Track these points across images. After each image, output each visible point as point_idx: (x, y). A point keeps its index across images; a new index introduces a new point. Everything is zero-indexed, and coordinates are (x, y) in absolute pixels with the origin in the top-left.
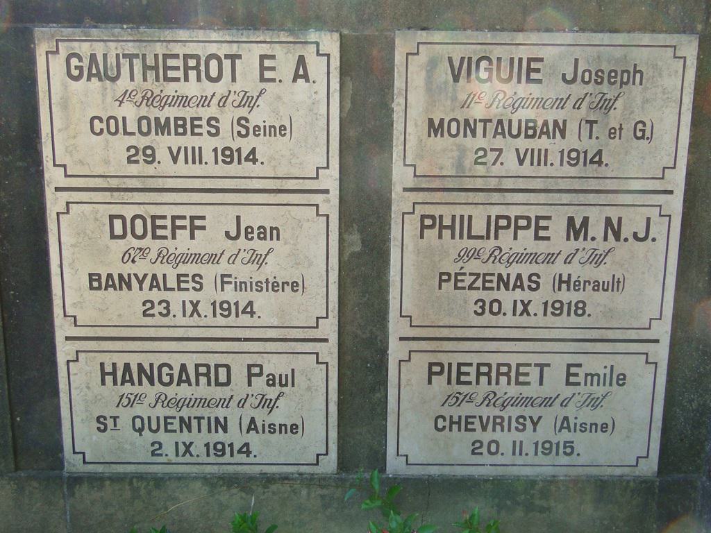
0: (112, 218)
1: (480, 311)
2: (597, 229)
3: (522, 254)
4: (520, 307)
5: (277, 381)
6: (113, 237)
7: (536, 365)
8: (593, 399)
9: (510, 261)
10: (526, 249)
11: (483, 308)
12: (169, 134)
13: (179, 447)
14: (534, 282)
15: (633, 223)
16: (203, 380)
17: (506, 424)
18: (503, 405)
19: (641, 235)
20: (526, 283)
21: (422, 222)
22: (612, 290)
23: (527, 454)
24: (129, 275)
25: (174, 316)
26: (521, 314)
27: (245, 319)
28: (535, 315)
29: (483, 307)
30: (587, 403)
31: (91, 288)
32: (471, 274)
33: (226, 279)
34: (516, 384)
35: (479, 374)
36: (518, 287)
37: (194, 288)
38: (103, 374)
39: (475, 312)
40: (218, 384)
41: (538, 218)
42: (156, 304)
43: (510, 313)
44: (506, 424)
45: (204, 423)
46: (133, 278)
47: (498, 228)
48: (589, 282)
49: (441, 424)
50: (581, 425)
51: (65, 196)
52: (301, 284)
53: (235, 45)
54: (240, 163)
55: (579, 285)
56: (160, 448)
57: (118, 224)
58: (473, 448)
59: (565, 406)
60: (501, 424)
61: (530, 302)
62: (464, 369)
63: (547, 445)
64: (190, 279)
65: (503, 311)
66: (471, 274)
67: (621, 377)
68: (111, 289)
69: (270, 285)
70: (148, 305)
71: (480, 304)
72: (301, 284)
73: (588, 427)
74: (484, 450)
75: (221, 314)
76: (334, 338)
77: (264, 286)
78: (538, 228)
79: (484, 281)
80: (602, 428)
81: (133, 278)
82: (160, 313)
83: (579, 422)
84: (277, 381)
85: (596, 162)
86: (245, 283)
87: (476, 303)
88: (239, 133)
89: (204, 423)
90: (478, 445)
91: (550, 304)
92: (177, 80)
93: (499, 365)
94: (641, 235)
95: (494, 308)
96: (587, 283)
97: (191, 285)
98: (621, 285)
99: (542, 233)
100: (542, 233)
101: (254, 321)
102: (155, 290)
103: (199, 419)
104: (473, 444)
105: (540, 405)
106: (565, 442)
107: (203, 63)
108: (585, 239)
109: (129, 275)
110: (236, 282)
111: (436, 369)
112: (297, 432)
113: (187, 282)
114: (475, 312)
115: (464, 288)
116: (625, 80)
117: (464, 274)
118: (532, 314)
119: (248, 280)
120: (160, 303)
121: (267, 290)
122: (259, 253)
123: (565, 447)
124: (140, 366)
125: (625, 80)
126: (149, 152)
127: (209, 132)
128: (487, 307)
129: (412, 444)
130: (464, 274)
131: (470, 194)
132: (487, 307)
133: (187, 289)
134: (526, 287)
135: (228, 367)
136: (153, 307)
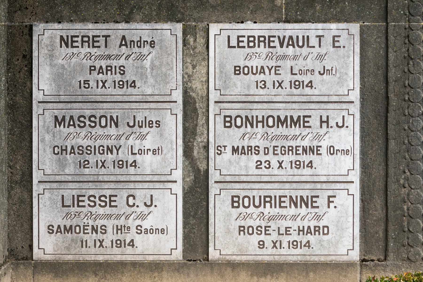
3: (279, 136)
9: (96, 139)
10: (281, 133)
13: (279, 246)
14: (80, 150)
15: (336, 118)
18: (268, 220)
19: (340, 124)
21: (225, 119)
22: (144, 154)
24: (112, 146)
25: (315, 168)
28: (286, 168)
30: (138, 218)
38: (322, 122)
42: (263, 163)
46: (114, 147)
48: (150, 150)
60: (111, 70)
61: (283, 161)
62: (283, 199)
68: (243, 155)
70: (259, 163)
80: (161, 231)
81: (114, 147)
82: (265, 167)
85: (309, 86)
91: (294, 162)
94: (340, 124)
96: (338, 151)
98: (160, 151)
105: (290, 220)
106: (85, 81)
109: (112, 146)
111: (93, 68)
112: (164, 233)
116: (139, 43)
120: (265, 162)
123: (84, 84)
125: (139, 43)
129: (226, 240)
134: (76, 153)
136: (261, 164)
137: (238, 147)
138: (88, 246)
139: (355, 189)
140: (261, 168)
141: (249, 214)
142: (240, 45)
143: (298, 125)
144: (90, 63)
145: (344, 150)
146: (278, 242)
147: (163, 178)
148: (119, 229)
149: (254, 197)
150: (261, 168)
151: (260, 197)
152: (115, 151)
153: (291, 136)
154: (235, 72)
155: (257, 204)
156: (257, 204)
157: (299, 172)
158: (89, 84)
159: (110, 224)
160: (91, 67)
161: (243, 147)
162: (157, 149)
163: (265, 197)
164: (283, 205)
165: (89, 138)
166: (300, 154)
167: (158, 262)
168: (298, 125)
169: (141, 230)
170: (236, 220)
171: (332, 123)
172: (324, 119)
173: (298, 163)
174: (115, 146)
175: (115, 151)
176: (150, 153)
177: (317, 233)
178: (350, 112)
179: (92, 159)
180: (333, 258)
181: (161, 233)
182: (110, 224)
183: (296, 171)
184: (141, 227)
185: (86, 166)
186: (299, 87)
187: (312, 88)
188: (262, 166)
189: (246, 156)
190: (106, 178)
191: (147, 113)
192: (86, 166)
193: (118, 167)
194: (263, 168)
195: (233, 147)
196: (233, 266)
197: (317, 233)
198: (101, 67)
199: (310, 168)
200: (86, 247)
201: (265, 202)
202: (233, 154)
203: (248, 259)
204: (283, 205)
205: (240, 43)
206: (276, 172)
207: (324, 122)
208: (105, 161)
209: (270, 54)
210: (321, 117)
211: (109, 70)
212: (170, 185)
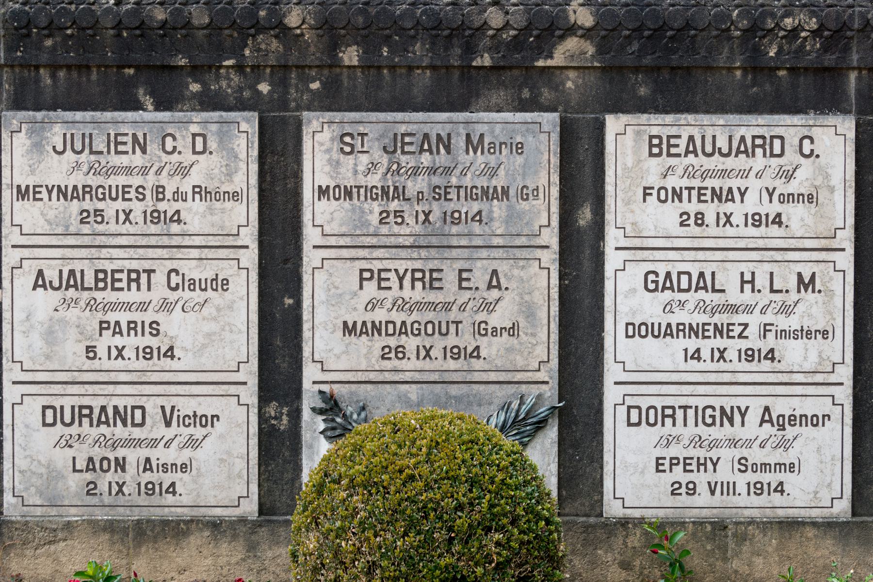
4: (717, 355)
5: (213, 195)
9: (106, 309)
12: (28, 200)
17: (139, 329)
23: (739, 494)
26: (116, 358)
28: (129, 359)
32: (739, 324)
33: (768, 328)
35: (130, 280)
36: (669, 335)
38: (743, 282)
40: (134, 425)
41: (380, 271)
42: (684, 486)
43: (413, 356)
44: (139, 329)
45: (691, 413)
48: (819, 331)
50: (163, 466)
53: (675, 128)
54: (767, 226)
56: (95, 488)
58: (86, 489)
60: (135, 329)
63: (150, 486)
66: (739, 324)
67: (792, 418)
68: (364, 336)
69: (804, 332)
73: (169, 467)
75: (746, 359)
76: (849, 383)
77: (799, 334)
78: (380, 279)
80: (182, 468)
83: (161, 462)
84: (213, 195)
86: (785, 331)
88: (434, 197)
89: (691, 413)
92: (126, 153)
93: (663, 408)
95: (400, 352)
99: (383, 284)
100: (383, 284)
103: (685, 408)
107: (768, 141)
108: (813, 291)
110: (777, 331)
115: (733, 337)
117: (734, 324)
118: (433, 358)
119: (787, 329)
121: (802, 338)
122: (169, 301)
124: (115, 408)
127: (137, 197)
130: (734, 324)
131: (707, 252)
133: (130, 200)
135: (143, 408)
137: (355, 323)
138: (737, 493)
139: (250, 257)
140: (680, 494)
142: (406, 150)
143: (810, 288)
144: (100, 316)
146: (716, 359)
148: (702, 464)
149: (62, 407)
151: (73, 407)
155: (68, 419)
156: (68, 419)
158: (102, 216)
159: (133, 456)
160: (101, 322)
161: (364, 323)
163: (81, 407)
166: (709, 337)
168: (810, 288)
169: (746, 466)
172: (748, 277)
176: (819, 336)
177: (681, 334)
181: (181, 471)
182: (133, 456)
183: (746, 366)
184: (747, 460)
185: (386, 356)
186: (459, 357)
187: (780, 226)
190: (484, 377)
192: (386, 356)
193: (144, 357)
194: (684, 494)
195: (345, 323)
197: (681, 334)
198: (117, 323)
200: (734, 494)
201: (81, 416)
202: (344, 335)
205: (672, 149)
206: (107, 364)
208: (431, 347)
210: (742, 274)
211: (197, 193)
212: (24, 241)
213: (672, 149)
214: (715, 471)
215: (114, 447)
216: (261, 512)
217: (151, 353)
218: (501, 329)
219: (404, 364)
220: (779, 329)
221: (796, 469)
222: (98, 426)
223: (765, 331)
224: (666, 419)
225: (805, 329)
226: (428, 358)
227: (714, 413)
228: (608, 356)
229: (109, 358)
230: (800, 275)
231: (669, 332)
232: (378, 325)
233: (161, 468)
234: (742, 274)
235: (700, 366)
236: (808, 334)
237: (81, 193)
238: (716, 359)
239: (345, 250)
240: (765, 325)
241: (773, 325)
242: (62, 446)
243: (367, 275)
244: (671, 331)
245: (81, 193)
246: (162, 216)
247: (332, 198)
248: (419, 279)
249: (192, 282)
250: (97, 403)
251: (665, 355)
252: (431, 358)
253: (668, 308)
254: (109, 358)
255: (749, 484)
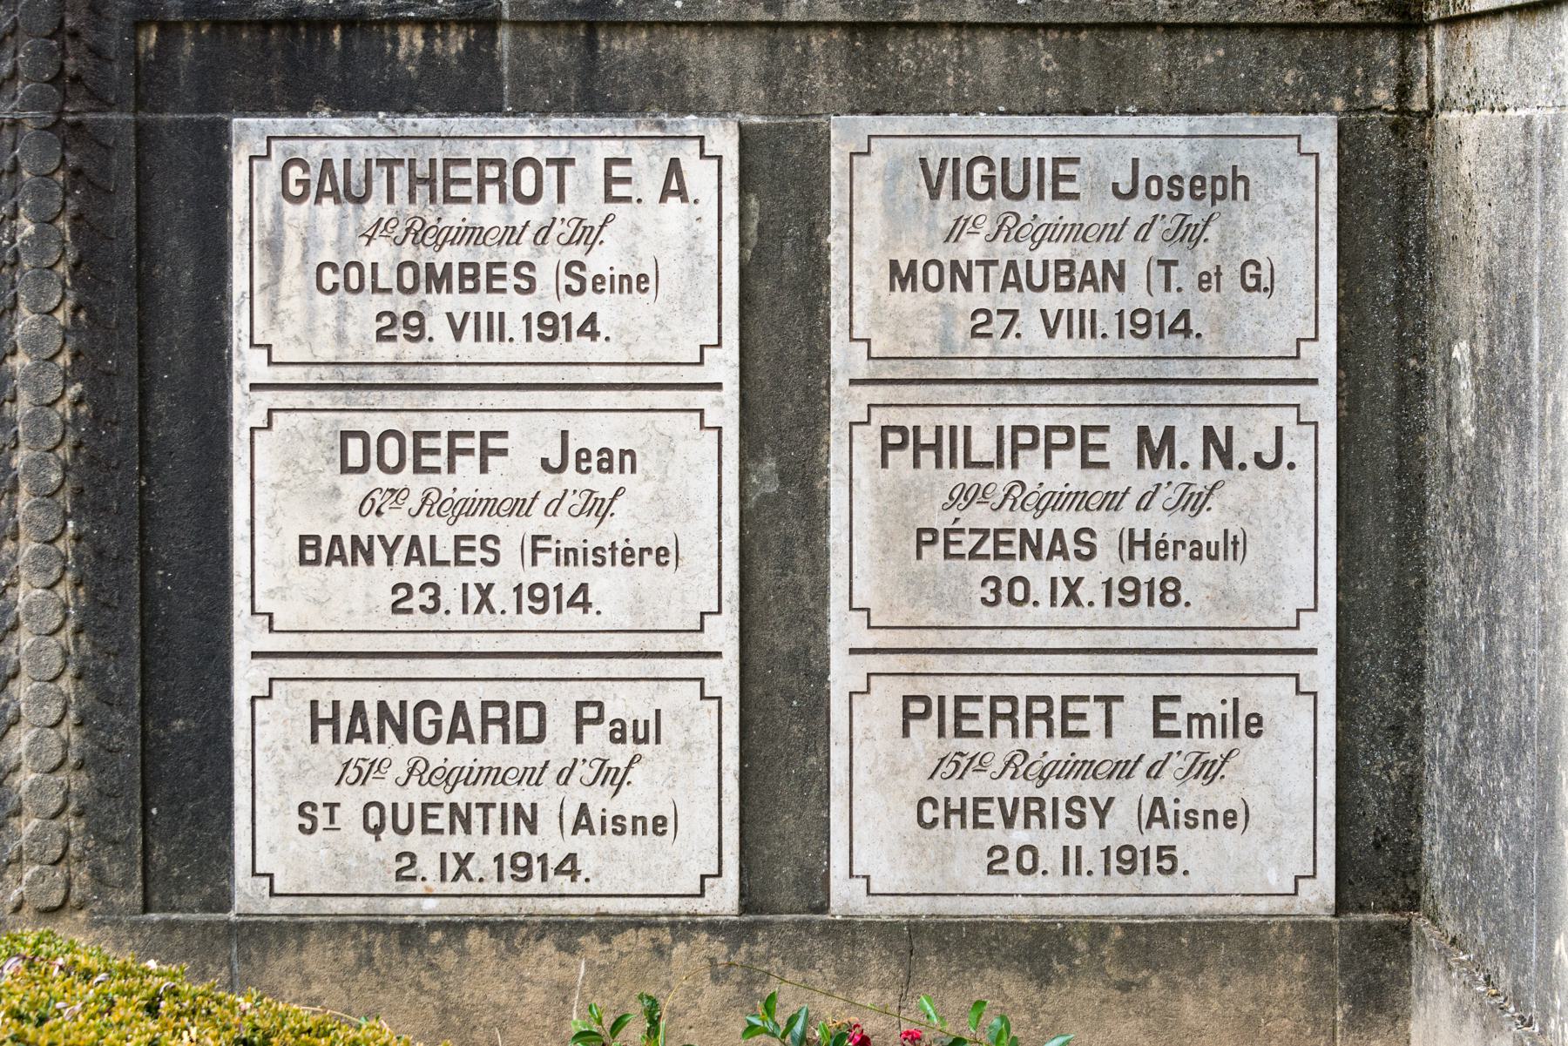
0: (345, 435)
1: (991, 598)
2: (1189, 447)
6: (346, 469)
7: (1098, 699)
8: (1204, 764)
11: (998, 592)
14: (576, 276)
15: (1253, 437)
16: (495, 732)
19: (1269, 458)
20: (1089, 811)
26: (1066, 603)
27: (572, 617)
28: (1091, 604)
29: (996, 591)
31: (303, 561)
32: (972, 531)
33: (540, 544)
34: (956, 735)
35: (995, 716)
37: (484, 561)
38: (316, 721)
39: (984, 600)
42: (416, 590)
45: (495, 814)
46: (376, 540)
47: (1016, 447)
48: (649, 550)
49: (929, 813)
51: (267, 399)
52: (672, 551)
55: (1166, 548)
57: (355, 446)
59: (1156, 777)
62: (967, 707)
64: (477, 543)
65: (1032, 599)
66: (972, 531)
71: (991, 585)
72: (672, 551)
73: (1200, 818)
74: (1011, 864)
77: (608, 555)
78: (1086, 447)
79: (997, 543)
80: (1226, 819)
81: (376, 540)
83: (1183, 808)
86: (575, 551)
87: (984, 584)
89: (495, 814)
90: (998, 855)
91: (1115, 584)
94: (1269, 458)
97: (479, 554)
98: (1240, 547)
99: (1093, 456)
101: (590, 621)
102: (415, 564)
103: (486, 807)
104: (990, 853)
105: (1109, 776)
108: (1171, 465)
109: (371, 537)
110: (558, 550)
113: (472, 549)
114: (984, 600)
116: (1219, 192)
119: (580, 547)
124: (382, 705)
126: (414, 321)
127: (517, 287)
128: (1004, 591)
132: (1004, 591)
133: (472, 563)
141: (972, 759)
142: (615, 193)
145: (1214, 812)
146: (472, 606)
147: (1269, 640)
150: (1005, 872)
152: (379, 553)
153: (1098, 496)
154: (302, 556)
157: (549, 619)
162: (607, 546)
164: (967, 725)
165: (434, 511)
167: (1251, 920)
170: (338, 783)
171: (1241, 453)
173: (1129, 586)
174: (382, 538)
175: (379, 553)
176: (649, 560)
178: (261, 421)
179: (451, 580)
180: (1219, 905)
183: (529, 620)
188: (413, 603)
189: (350, 568)
191: (1229, 689)
196: (294, 930)
199: (580, 610)
203: (1141, 911)
204: (967, 725)
205: (1061, 184)
207: (1218, 447)
209: (1011, 221)
213: (1061, 184)
214: (1102, 825)
215: (1042, 779)
216: (745, 908)
217: (1136, 591)
218: (642, 550)
219: (1027, 615)
220: (562, 546)
221: (670, 827)
222: (349, 741)
223: (535, 550)
224: (321, 728)
225: (620, 545)
226: (1072, 604)
227: (438, 717)
228: (240, 603)
229: (465, 611)
230: (1143, 432)
231: (362, 550)
232: (360, 557)
233: (609, 826)
234: (314, 704)
235: (1083, 616)
236: (628, 556)
237: (1099, 274)
238: (472, 606)
239: (1131, 388)
240: (535, 538)
241: (548, 538)
242: (352, 780)
243: (1025, 438)
244: (342, 549)
245: (1099, 274)
246: (1155, 320)
247: (920, 285)
248: (1004, 716)
249: (583, 455)
250: (446, 697)
251: (358, 595)
252: (1078, 603)
253: (369, 506)
254: (465, 611)
255: (1107, 851)
